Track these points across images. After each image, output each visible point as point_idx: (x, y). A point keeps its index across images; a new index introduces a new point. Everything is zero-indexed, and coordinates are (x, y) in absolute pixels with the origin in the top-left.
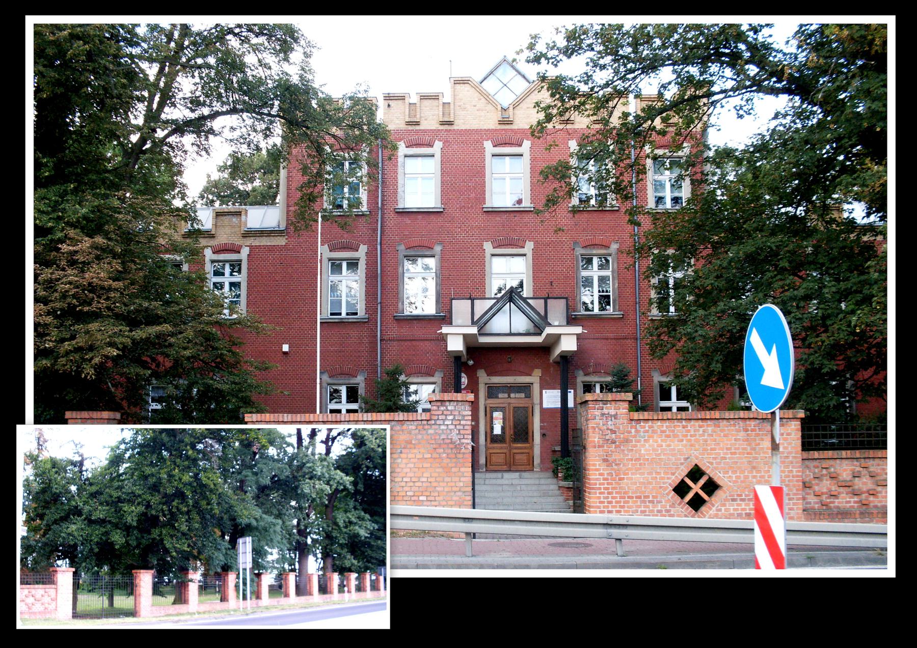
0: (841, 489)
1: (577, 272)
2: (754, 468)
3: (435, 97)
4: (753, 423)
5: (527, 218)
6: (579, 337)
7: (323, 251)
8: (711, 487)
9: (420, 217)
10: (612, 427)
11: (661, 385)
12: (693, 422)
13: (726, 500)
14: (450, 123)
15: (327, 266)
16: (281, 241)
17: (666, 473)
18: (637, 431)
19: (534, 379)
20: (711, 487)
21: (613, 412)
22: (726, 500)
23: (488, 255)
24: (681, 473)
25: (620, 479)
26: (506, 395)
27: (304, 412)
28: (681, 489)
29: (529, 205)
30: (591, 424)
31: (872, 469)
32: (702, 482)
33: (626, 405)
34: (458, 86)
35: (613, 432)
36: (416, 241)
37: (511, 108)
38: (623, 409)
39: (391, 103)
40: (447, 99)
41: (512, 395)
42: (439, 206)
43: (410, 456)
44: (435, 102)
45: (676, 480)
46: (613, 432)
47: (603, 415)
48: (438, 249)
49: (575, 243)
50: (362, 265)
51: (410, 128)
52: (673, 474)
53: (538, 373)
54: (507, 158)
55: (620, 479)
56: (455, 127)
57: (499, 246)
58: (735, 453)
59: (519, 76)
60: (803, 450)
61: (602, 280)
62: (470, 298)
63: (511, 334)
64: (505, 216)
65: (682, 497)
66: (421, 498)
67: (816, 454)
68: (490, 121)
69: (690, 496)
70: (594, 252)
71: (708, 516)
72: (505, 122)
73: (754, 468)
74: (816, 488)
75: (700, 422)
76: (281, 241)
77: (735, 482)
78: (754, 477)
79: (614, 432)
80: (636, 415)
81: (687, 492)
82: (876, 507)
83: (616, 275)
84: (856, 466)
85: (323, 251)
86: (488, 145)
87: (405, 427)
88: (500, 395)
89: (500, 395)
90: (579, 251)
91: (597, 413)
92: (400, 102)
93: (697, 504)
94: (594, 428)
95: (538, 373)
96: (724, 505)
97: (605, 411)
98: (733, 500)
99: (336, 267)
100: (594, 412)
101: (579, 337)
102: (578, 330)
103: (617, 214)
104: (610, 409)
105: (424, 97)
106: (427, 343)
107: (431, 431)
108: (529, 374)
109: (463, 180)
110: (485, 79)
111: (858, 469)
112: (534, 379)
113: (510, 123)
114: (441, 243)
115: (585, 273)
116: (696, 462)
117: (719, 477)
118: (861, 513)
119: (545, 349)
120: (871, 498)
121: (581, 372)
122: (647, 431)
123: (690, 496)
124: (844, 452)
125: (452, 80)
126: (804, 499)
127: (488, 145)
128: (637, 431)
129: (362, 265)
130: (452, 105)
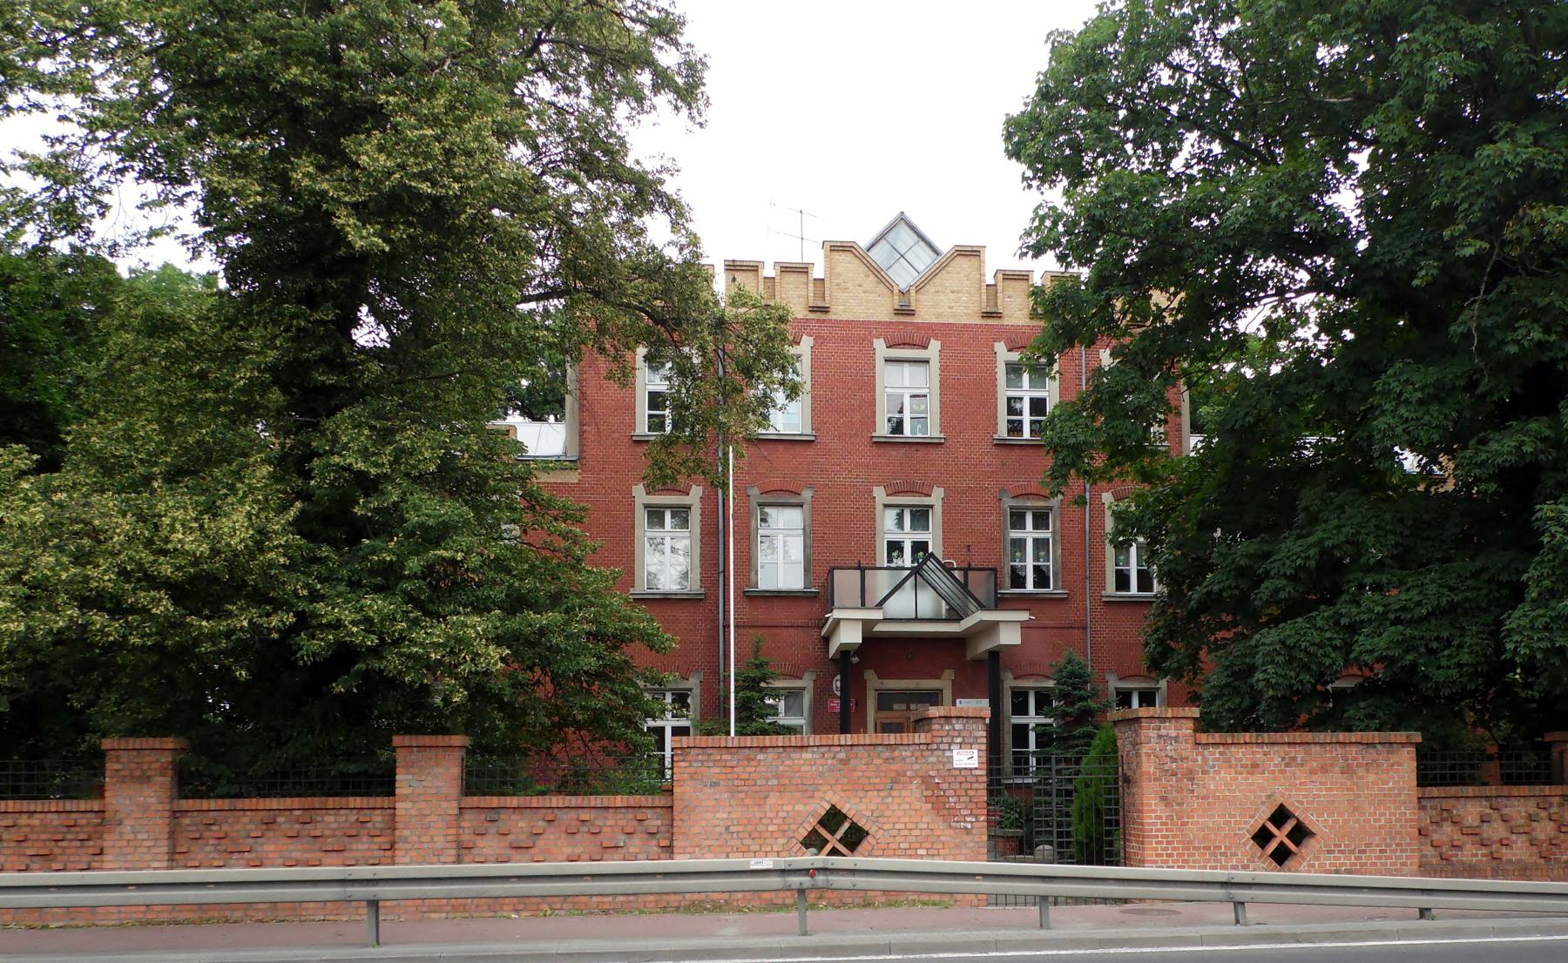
0: (1465, 838)
1: (1004, 533)
2: (1356, 809)
3: (803, 270)
4: (1354, 749)
5: (935, 454)
6: (1025, 626)
7: (640, 495)
8: (1301, 833)
9: (781, 447)
10: (1173, 754)
11: (1119, 692)
12: (1276, 748)
13: (1320, 851)
14: (825, 310)
15: (641, 516)
16: (573, 478)
17: (1242, 815)
18: (1205, 760)
19: (944, 683)
20: (1301, 833)
21: (1173, 733)
22: (1320, 851)
23: (879, 507)
24: (1262, 816)
25: (1184, 824)
26: (904, 707)
27: (827, 733)
28: (1262, 837)
29: (937, 435)
30: (1145, 749)
31: (1505, 811)
32: (1288, 827)
33: (1190, 724)
34: (836, 255)
35: (1174, 760)
36: (775, 482)
37: (913, 292)
38: (1187, 729)
39: (737, 274)
40: (818, 272)
41: (913, 706)
42: (809, 431)
43: (904, 793)
44: (802, 278)
45: (1255, 823)
46: (1174, 760)
47: (1160, 736)
48: (807, 495)
49: (1003, 491)
50: (695, 517)
51: (984, 322)
52: (1252, 817)
53: (949, 675)
54: (906, 366)
55: (1184, 824)
56: (831, 316)
57: (895, 493)
58: (1330, 790)
59: (922, 244)
60: (1419, 785)
61: (1040, 544)
62: (859, 568)
63: (917, 620)
64: (903, 450)
65: (1263, 847)
66: (920, 852)
67: (1434, 791)
68: (881, 309)
69: (1273, 846)
70: (1029, 504)
71: (1297, 872)
72: (905, 311)
73: (1356, 809)
74: (1435, 837)
75: (1286, 748)
76: (573, 478)
77: (1331, 828)
78: (1356, 821)
79: (1175, 760)
80: (1203, 737)
81: (840, 824)
82: (1510, 861)
83: (1058, 538)
84: (1531, 806)
85: (640, 495)
86: (879, 345)
87: (897, 753)
88: (895, 706)
89: (895, 706)
90: (1008, 502)
91: (1153, 734)
92: (750, 274)
93: (1281, 856)
94: (1148, 755)
95: (949, 675)
96: (1318, 859)
97: (1163, 732)
98: (1329, 852)
99: (656, 515)
100: (1149, 732)
101: (1025, 626)
102: (1024, 616)
103: (940, 451)
104: (1170, 730)
105: (786, 269)
106: (792, 631)
107: (932, 759)
108: (938, 677)
109: (847, 394)
110: (873, 245)
111: (1488, 811)
112: (944, 683)
113: (911, 313)
114: (811, 486)
115: (1015, 534)
116: (1281, 800)
117: (1311, 821)
118: (1493, 869)
119: (958, 643)
120: (1504, 850)
121: (1009, 675)
122: (1217, 760)
123: (1273, 846)
124: (1470, 789)
125: (827, 246)
126: (1420, 850)
127: (879, 345)
128: (1205, 760)
129: (695, 517)
130: (827, 284)
